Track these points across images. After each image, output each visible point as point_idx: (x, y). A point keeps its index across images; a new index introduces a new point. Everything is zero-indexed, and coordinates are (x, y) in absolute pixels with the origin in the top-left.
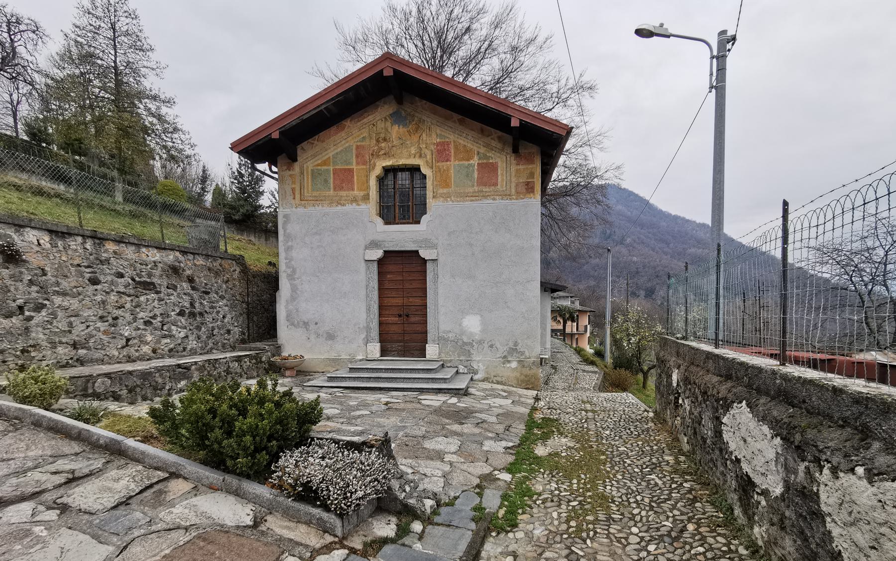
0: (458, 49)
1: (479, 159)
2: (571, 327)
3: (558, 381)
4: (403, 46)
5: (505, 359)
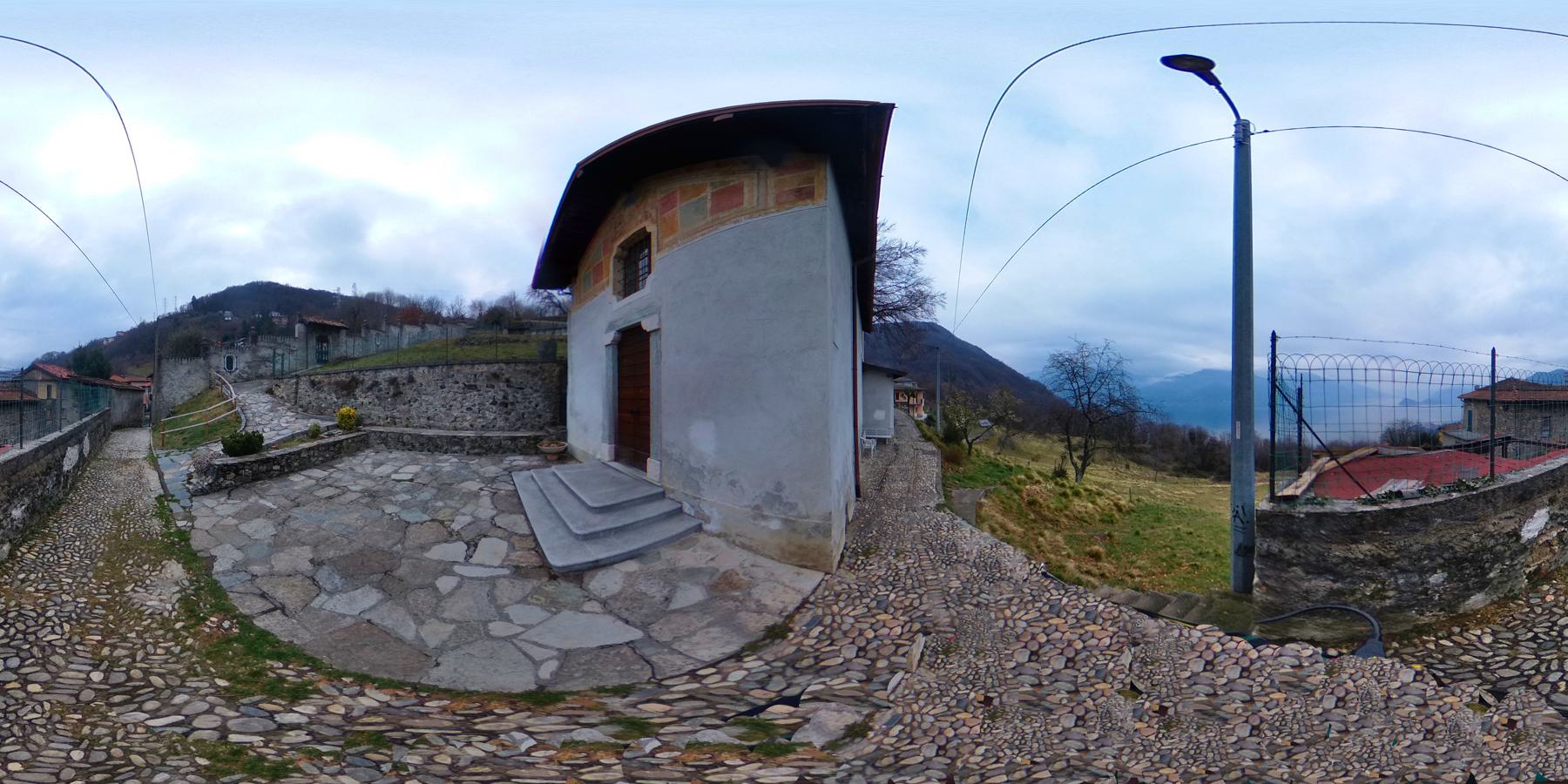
5: (758, 513)
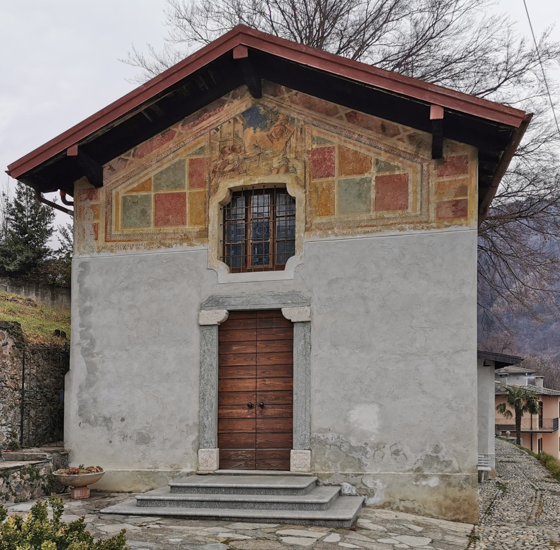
0: (348, 12)
1: (378, 172)
2: (528, 422)
3: (507, 508)
4: (262, 13)
5: (419, 474)
